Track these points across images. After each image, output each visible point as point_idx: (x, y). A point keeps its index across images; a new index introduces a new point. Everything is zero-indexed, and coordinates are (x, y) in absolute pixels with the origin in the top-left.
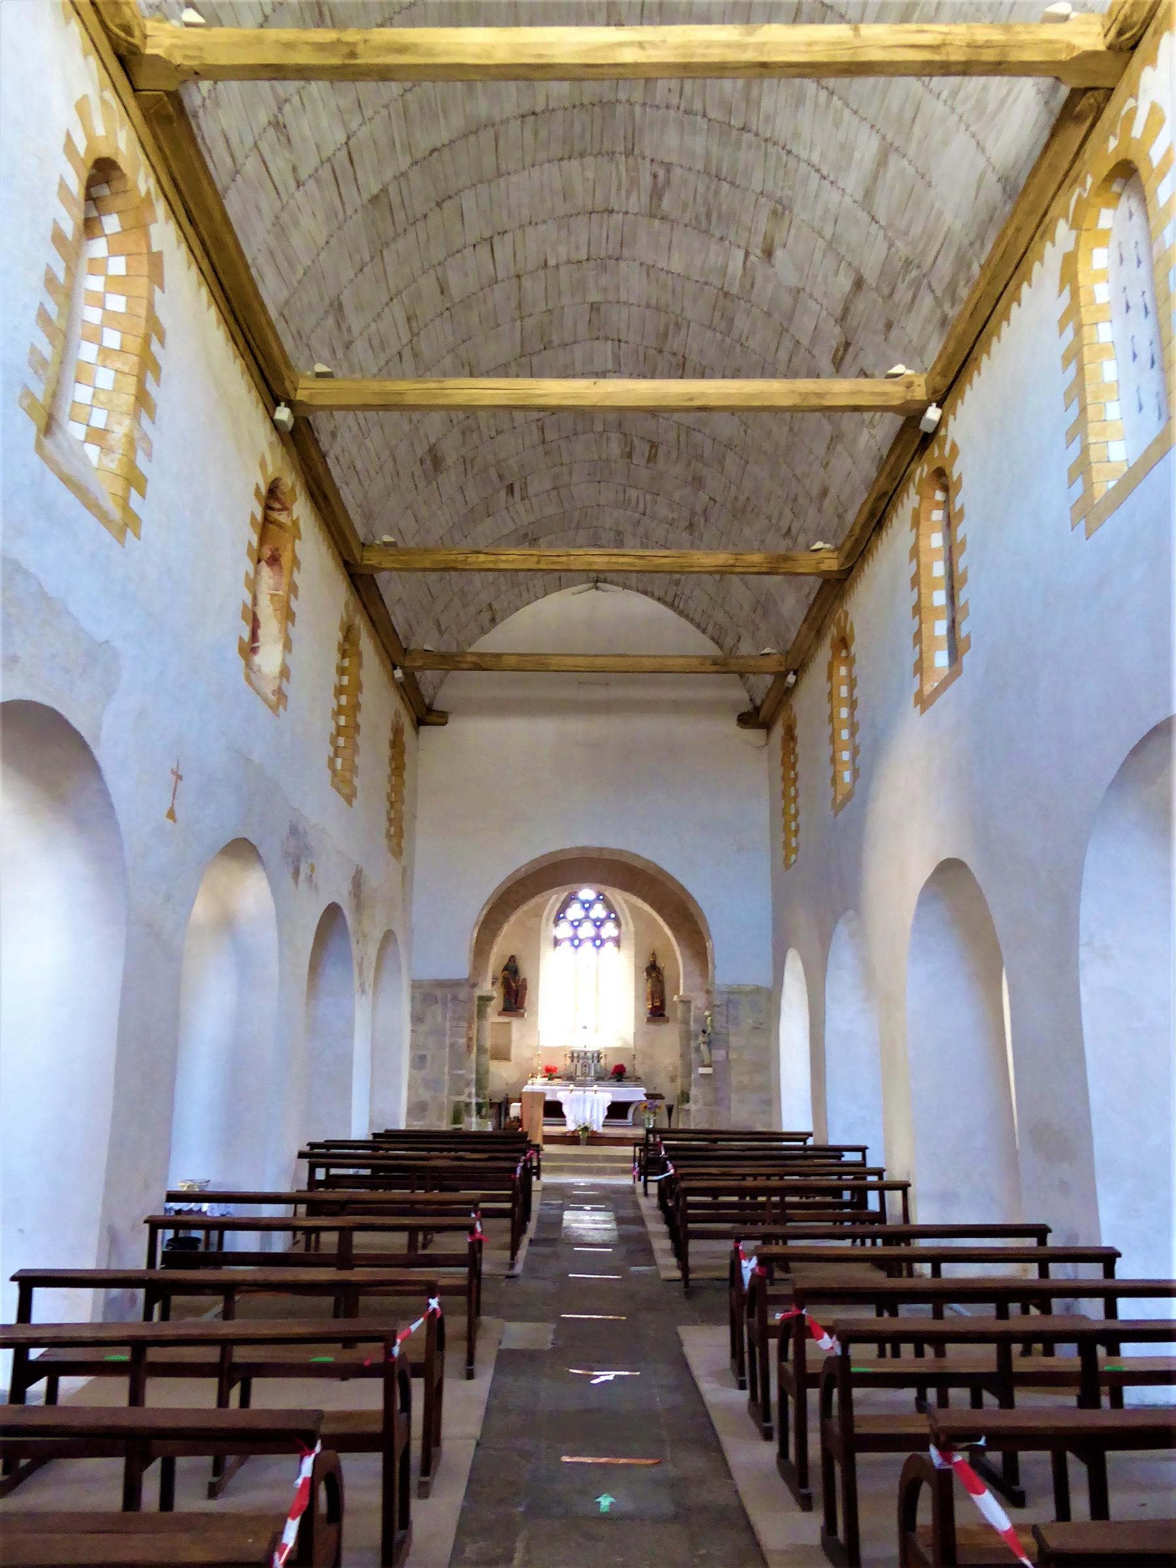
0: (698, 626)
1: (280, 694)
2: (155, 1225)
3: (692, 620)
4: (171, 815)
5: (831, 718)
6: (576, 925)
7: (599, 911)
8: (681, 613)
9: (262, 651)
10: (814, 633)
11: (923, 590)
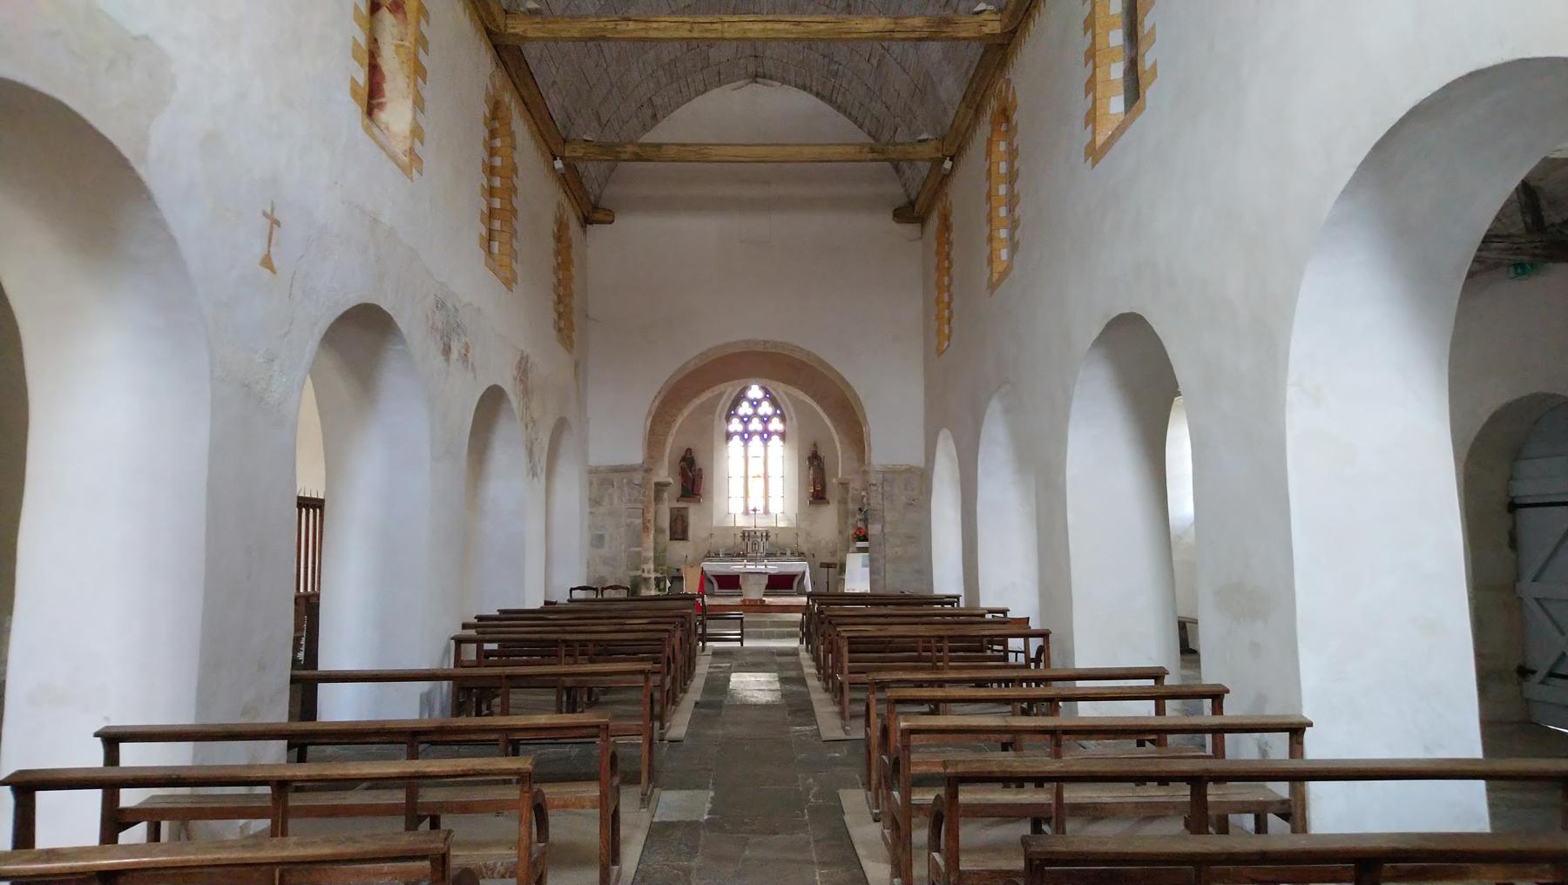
0: (855, 121)
1: (415, 158)
2: (459, 641)
3: (849, 116)
4: (267, 262)
5: (989, 197)
6: (745, 420)
7: (766, 408)
8: (839, 108)
9: (389, 108)
10: (972, 112)
11: (1098, 30)
